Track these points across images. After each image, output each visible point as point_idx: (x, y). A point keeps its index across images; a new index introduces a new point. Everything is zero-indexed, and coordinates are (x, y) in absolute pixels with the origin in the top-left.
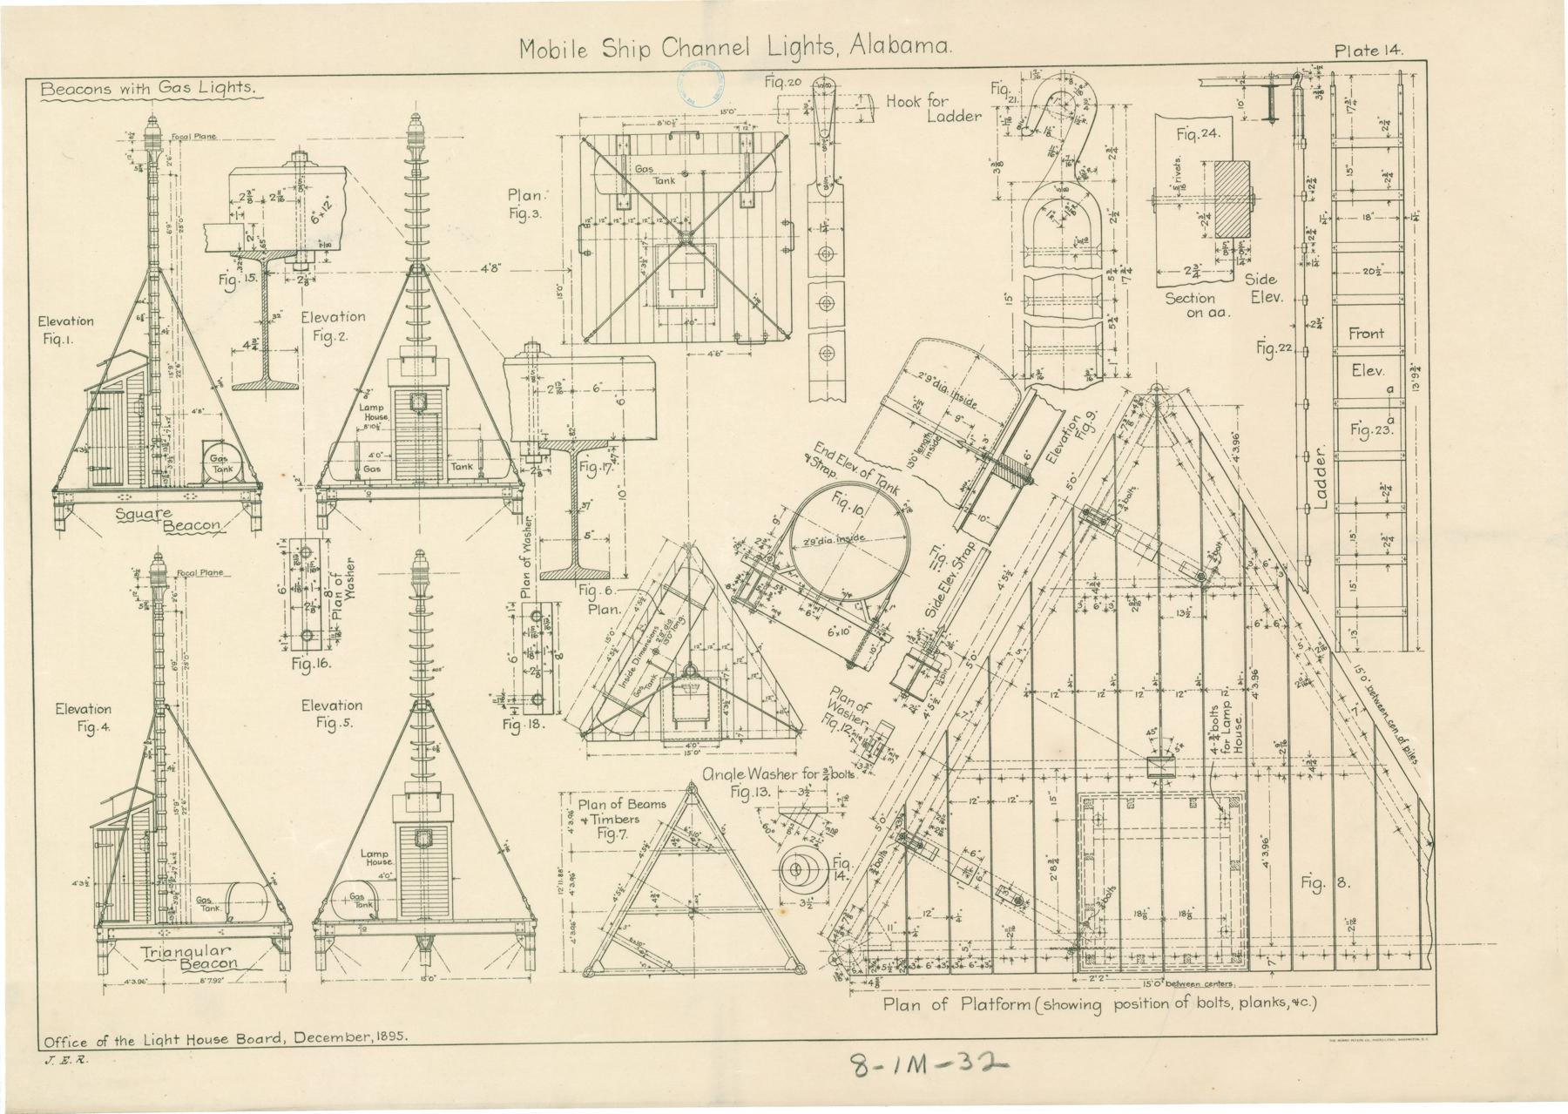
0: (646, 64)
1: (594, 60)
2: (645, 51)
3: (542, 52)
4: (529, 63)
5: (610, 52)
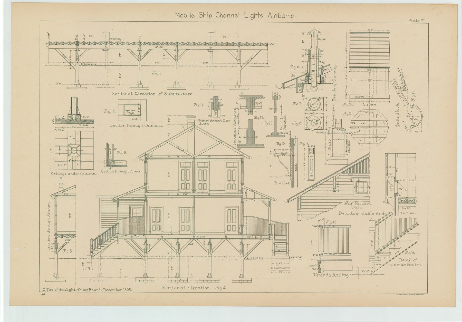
0: (211, 19)
1: (196, 18)
2: (211, 16)
3: (182, 16)
4: (178, 19)
5: (201, 16)
